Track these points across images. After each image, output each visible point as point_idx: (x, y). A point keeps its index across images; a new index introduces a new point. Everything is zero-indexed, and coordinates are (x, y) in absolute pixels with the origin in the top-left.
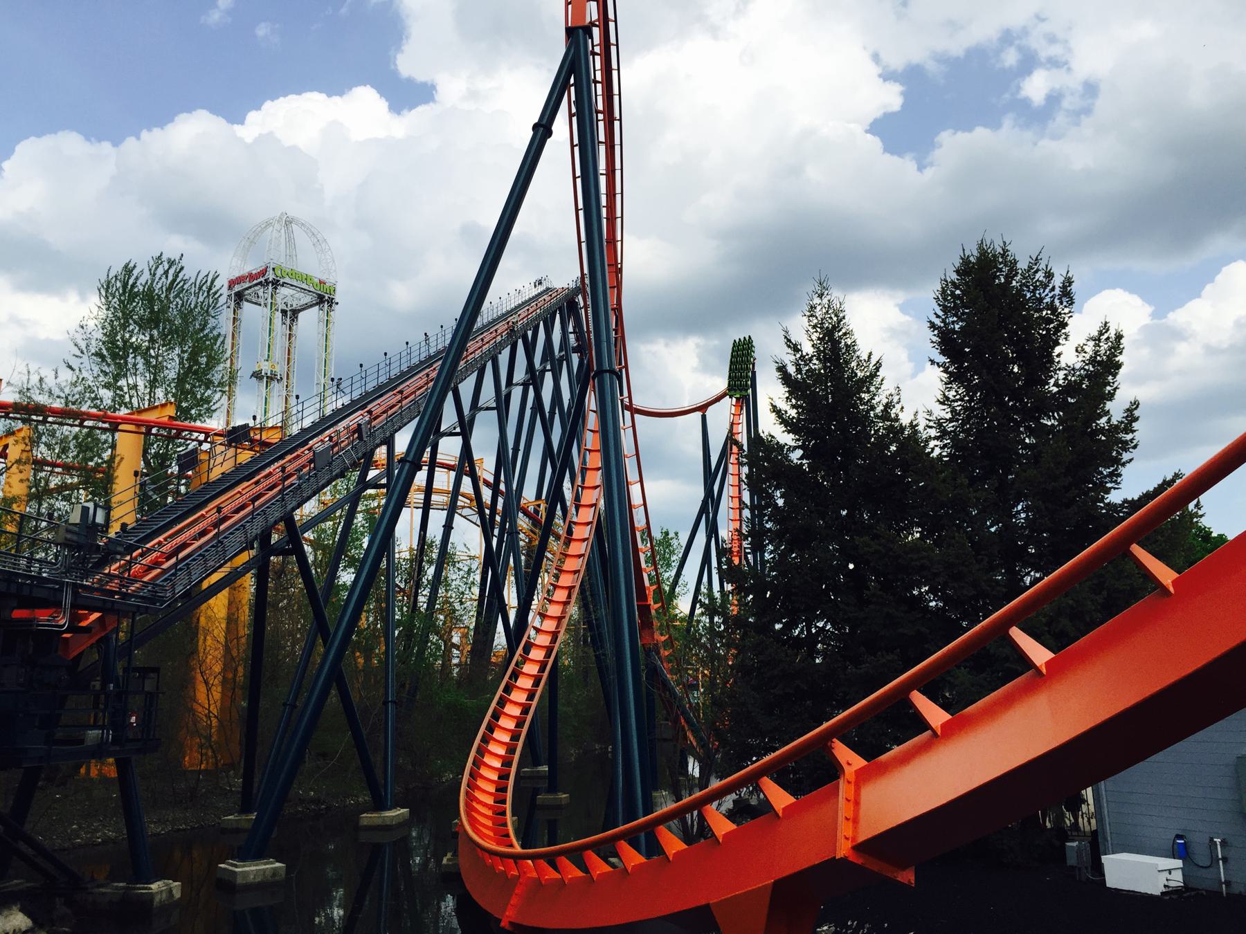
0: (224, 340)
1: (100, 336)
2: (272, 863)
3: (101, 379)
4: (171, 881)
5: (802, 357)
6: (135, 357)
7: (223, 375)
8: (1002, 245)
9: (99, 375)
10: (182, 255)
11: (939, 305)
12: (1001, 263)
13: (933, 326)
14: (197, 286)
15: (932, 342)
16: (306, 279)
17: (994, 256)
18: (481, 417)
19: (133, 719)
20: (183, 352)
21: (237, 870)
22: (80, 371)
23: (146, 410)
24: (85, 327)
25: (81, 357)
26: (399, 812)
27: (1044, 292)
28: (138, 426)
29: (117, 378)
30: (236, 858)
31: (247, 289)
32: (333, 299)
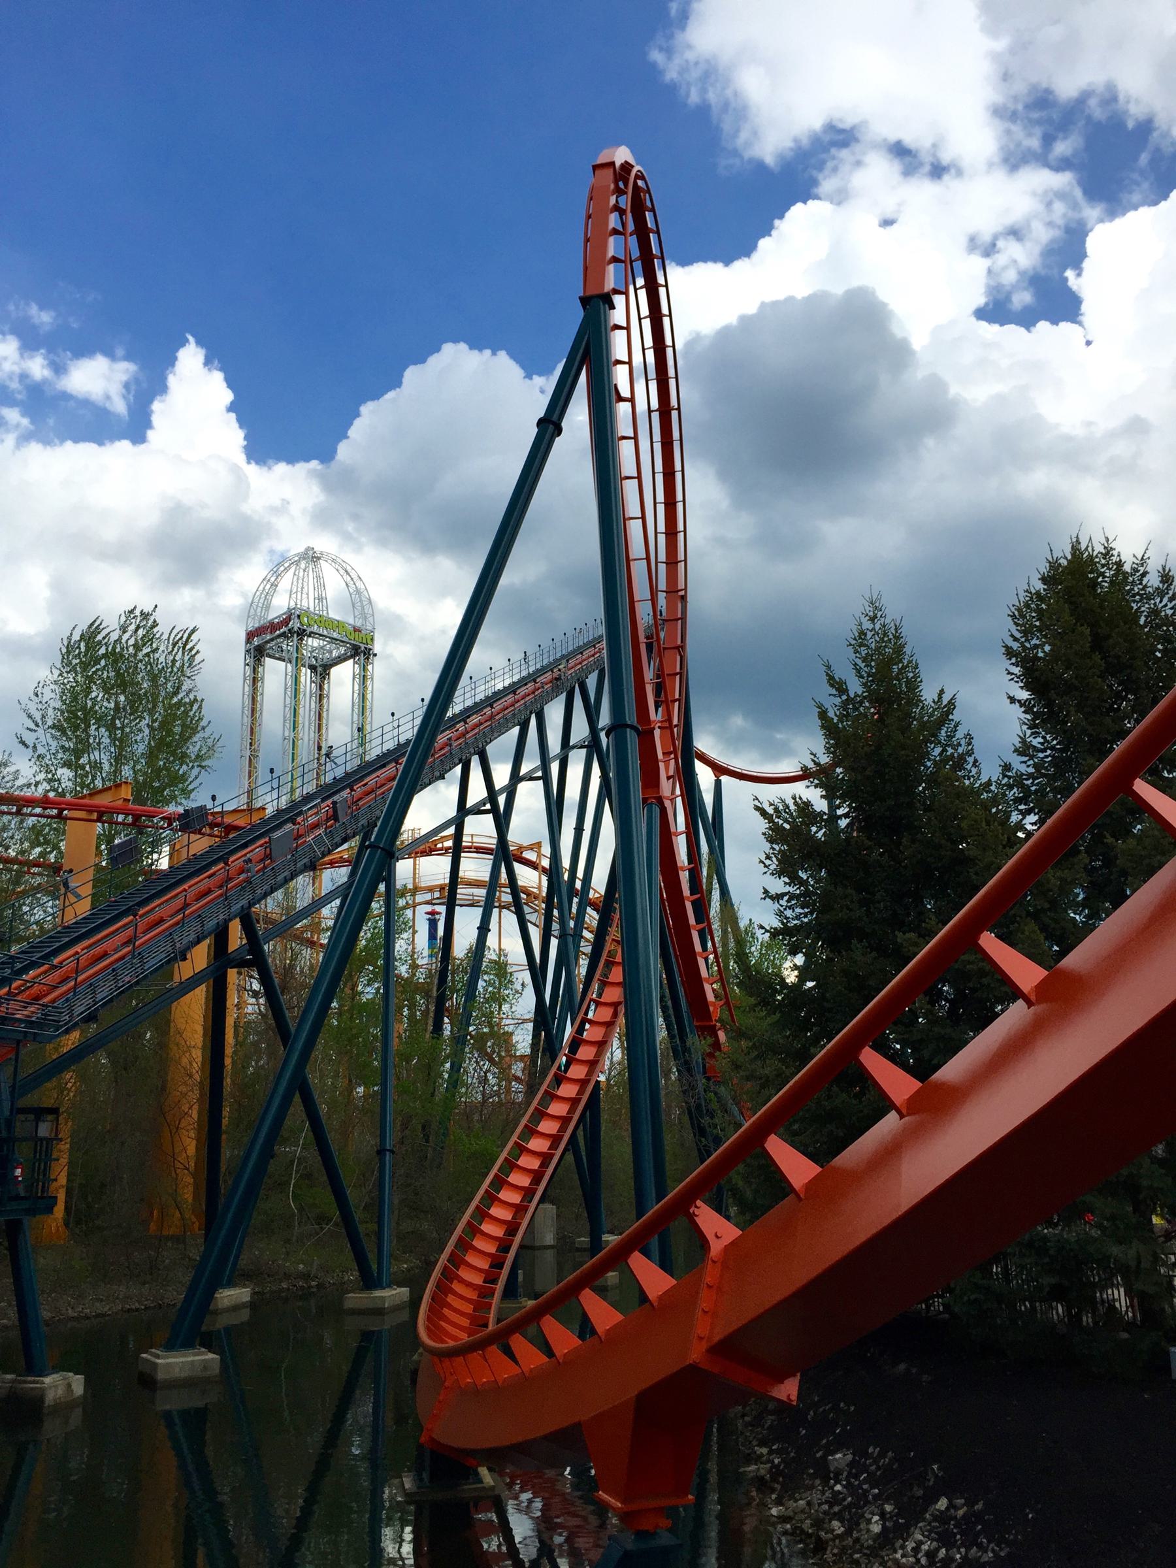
0: (201, 705)
1: (58, 704)
2: (203, 1354)
3: (60, 756)
4: (71, 1374)
5: (849, 700)
6: (97, 729)
7: (201, 746)
8: (1104, 541)
9: (57, 752)
10: (156, 606)
11: (1017, 624)
12: (1103, 566)
13: (1009, 653)
14: (171, 641)
15: (1009, 673)
16: (338, 625)
17: (1091, 557)
18: (523, 788)
19: (18, 1172)
20: (154, 721)
21: (159, 1361)
22: (35, 747)
23: (101, 792)
24: (40, 695)
25: (35, 731)
26: (394, 1292)
27: (1161, 602)
28: (90, 812)
29: (78, 753)
30: (161, 1346)
31: (268, 642)
32: (370, 649)
